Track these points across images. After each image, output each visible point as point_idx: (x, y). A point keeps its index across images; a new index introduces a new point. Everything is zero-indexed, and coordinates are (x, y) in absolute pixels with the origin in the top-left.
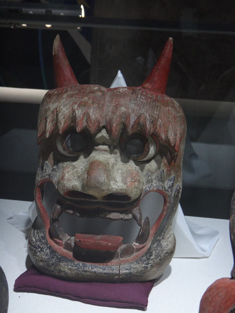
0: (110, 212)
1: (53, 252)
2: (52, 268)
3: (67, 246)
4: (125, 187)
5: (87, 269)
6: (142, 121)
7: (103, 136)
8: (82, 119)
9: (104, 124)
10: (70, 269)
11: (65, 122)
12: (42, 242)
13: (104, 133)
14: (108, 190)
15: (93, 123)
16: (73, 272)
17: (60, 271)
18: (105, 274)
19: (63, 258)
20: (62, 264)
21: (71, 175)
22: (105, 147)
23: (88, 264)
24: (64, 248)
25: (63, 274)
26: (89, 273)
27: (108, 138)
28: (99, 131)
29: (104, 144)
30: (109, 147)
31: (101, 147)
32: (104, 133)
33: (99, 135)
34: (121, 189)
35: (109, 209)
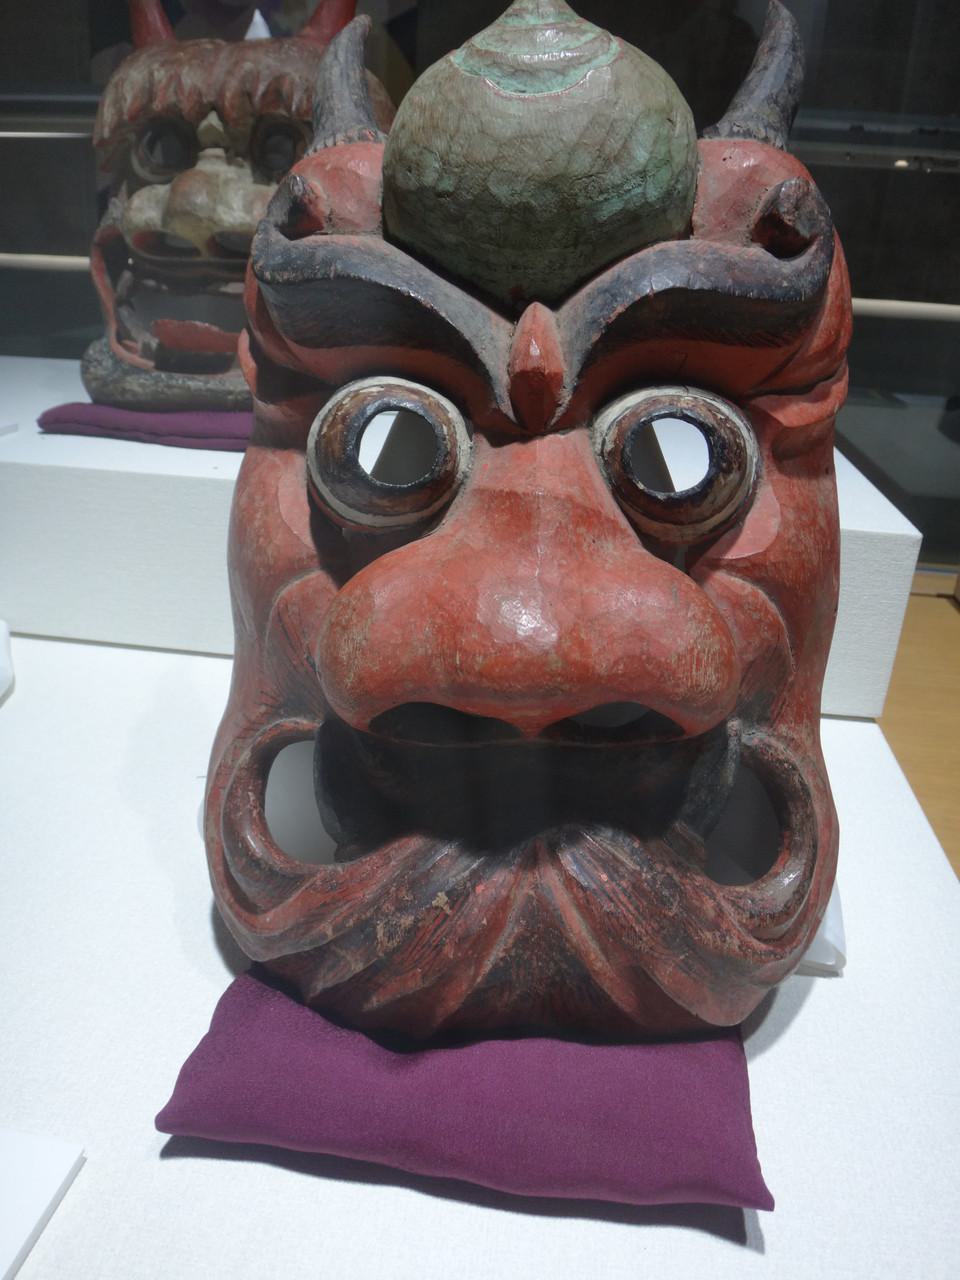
0: (227, 281)
1: (118, 362)
2: (111, 387)
3: (146, 352)
4: (248, 219)
5: (174, 382)
6: (286, 88)
7: (211, 127)
8: (167, 87)
9: (212, 99)
10: (142, 385)
11: (135, 98)
12: (789, 844)
13: (213, 119)
14: (211, 219)
15: (186, 94)
16: (148, 390)
17: (124, 391)
18: (208, 390)
19: (137, 370)
20: (129, 379)
21: (144, 208)
22: (219, 152)
23: (176, 375)
24: (142, 357)
25: (129, 397)
26: (176, 391)
27: (221, 129)
28: (204, 116)
29: (216, 145)
30: (227, 150)
31: (210, 151)
32: (213, 119)
33: (204, 124)
34: (242, 225)
35: (437, 505)
